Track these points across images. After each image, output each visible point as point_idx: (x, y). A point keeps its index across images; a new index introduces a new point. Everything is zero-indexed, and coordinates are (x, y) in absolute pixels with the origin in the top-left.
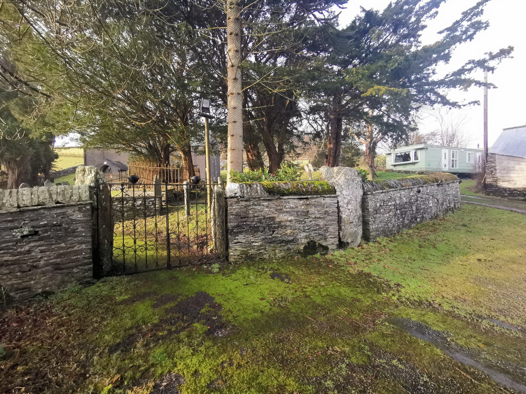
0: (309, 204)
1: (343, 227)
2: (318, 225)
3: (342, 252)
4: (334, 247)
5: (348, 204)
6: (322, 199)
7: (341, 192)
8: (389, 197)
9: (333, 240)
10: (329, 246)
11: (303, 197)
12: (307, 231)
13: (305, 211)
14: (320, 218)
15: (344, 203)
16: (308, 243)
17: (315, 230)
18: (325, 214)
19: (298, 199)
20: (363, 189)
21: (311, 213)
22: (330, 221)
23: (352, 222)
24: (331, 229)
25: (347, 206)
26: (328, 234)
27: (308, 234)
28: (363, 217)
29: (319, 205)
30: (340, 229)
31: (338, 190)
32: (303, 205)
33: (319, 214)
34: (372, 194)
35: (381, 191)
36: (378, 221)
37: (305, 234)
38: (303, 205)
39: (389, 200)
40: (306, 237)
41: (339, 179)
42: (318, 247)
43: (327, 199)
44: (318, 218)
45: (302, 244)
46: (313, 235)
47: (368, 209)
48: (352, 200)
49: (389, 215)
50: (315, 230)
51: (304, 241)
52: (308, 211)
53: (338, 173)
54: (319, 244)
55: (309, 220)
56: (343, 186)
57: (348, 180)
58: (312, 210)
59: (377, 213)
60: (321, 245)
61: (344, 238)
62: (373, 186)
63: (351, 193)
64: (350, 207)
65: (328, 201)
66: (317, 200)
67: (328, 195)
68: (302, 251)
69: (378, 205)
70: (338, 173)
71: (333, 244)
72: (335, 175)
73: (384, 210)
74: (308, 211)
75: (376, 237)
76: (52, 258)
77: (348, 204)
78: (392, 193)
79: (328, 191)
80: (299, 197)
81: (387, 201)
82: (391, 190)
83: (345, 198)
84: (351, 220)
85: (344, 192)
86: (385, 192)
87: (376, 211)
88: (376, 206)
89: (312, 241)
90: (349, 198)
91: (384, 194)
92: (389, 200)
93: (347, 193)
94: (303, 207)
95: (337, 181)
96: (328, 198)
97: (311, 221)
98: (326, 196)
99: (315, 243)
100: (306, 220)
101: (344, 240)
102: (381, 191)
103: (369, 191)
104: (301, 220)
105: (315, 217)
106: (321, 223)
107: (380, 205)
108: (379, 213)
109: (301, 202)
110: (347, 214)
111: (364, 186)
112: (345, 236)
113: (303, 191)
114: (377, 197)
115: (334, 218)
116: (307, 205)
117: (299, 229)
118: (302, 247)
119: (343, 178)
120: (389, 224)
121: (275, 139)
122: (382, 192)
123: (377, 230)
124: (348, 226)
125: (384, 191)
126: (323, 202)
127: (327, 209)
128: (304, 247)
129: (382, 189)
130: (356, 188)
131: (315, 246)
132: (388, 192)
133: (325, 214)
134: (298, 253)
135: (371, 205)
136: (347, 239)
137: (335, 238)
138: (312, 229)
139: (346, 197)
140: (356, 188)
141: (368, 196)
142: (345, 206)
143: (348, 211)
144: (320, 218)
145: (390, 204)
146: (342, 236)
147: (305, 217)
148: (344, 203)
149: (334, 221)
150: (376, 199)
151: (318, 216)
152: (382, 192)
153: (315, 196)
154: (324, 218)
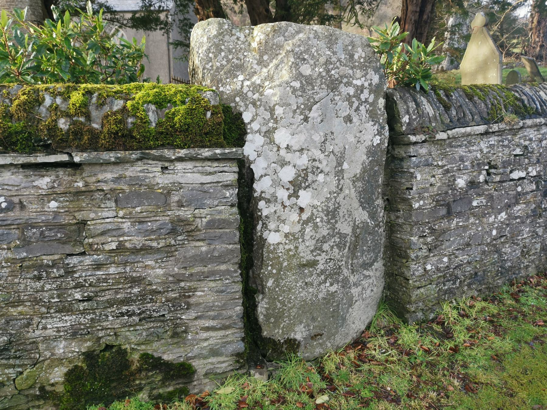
0: (87, 192)
1: (270, 283)
2: (135, 281)
3: (258, 382)
4: (223, 363)
5: (297, 185)
6: (155, 168)
7: (269, 134)
8: (518, 151)
9: (215, 338)
10: (195, 364)
11: (42, 158)
12: (82, 306)
13: (65, 220)
14: (145, 250)
15: (277, 183)
16: (89, 356)
17: (126, 301)
18: (173, 232)
19: (25, 166)
20: (392, 118)
21: (101, 228)
22: (203, 259)
23: (313, 264)
24: (205, 293)
25: (295, 195)
26: (192, 314)
27: (85, 320)
28: (392, 228)
29: (139, 195)
30: (250, 294)
31: (255, 126)
32: (52, 194)
33: (139, 232)
34: (431, 140)
35: (482, 128)
36: (452, 244)
37: (69, 320)
38: (52, 194)
39: (515, 162)
40: (75, 333)
41: (270, 78)
42: (140, 370)
43: (179, 166)
44: (135, 251)
45: (60, 361)
46: (111, 322)
47: (406, 201)
48: (317, 171)
49: (511, 217)
50: (126, 301)
51: (69, 350)
52: (84, 223)
53: (269, 49)
54: (145, 357)
55: (88, 260)
56: (279, 111)
57: (309, 81)
58: (103, 216)
59: (449, 214)
60: (153, 363)
61: (276, 324)
62: (447, 108)
63: (318, 138)
64: (305, 198)
65: (191, 174)
66: (132, 171)
67: (182, 152)
68: (60, 389)
69: (461, 182)
70: (269, 49)
71: (214, 352)
72: (251, 59)
73: (490, 198)
74: (84, 223)
75: (439, 302)
76: (76, 206)
77: (297, 185)
78: (532, 134)
79: (185, 129)
80: (22, 159)
81: (505, 164)
82: (529, 122)
83: (283, 163)
84: (306, 256)
85: (282, 137)
86: (500, 133)
87: (450, 204)
88: (452, 185)
89: (109, 347)
90: (303, 161)
91: (493, 140)
92: (515, 162)
93: (295, 143)
94: (53, 204)
95: (257, 88)
96: (189, 165)
97: (98, 266)
98: (168, 153)
99: (122, 353)
100: (74, 260)
101: (272, 331)
102: (482, 128)
103: (422, 129)
104: (47, 260)
105: (121, 248)
106: (155, 271)
107: (472, 184)
108: (459, 214)
109: (44, 182)
110: (286, 229)
111: (401, 107)
112: (279, 317)
113: (53, 129)
114: (461, 151)
115: (220, 247)
116: (78, 193)
117: (37, 301)
118: (57, 375)
119: (285, 74)
120: (507, 249)
121: (433, 40)
122: (486, 133)
123: (448, 275)
124: (290, 278)
125: (495, 127)
126: (162, 180)
127: (186, 213)
128: (68, 374)
129: (486, 122)
130: (348, 119)
131: (126, 364)
132: (514, 132)
133: (173, 232)
134: (38, 398)
135: (424, 181)
136: (290, 328)
137: (225, 328)
138: (108, 296)
139: (288, 157)
140: (348, 119)
141: (412, 150)
142: (282, 194)
143: (294, 217)
144: (145, 250)
145: (516, 175)
146: (267, 316)
147: (68, 249)
148: (277, 183)
149: (221, 259)
150: (452, 161)
151: (138, 241)
152: (486, 133)
153: (111, 156)
154: (168, 251)
